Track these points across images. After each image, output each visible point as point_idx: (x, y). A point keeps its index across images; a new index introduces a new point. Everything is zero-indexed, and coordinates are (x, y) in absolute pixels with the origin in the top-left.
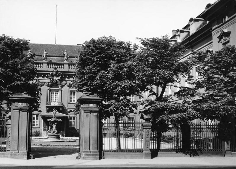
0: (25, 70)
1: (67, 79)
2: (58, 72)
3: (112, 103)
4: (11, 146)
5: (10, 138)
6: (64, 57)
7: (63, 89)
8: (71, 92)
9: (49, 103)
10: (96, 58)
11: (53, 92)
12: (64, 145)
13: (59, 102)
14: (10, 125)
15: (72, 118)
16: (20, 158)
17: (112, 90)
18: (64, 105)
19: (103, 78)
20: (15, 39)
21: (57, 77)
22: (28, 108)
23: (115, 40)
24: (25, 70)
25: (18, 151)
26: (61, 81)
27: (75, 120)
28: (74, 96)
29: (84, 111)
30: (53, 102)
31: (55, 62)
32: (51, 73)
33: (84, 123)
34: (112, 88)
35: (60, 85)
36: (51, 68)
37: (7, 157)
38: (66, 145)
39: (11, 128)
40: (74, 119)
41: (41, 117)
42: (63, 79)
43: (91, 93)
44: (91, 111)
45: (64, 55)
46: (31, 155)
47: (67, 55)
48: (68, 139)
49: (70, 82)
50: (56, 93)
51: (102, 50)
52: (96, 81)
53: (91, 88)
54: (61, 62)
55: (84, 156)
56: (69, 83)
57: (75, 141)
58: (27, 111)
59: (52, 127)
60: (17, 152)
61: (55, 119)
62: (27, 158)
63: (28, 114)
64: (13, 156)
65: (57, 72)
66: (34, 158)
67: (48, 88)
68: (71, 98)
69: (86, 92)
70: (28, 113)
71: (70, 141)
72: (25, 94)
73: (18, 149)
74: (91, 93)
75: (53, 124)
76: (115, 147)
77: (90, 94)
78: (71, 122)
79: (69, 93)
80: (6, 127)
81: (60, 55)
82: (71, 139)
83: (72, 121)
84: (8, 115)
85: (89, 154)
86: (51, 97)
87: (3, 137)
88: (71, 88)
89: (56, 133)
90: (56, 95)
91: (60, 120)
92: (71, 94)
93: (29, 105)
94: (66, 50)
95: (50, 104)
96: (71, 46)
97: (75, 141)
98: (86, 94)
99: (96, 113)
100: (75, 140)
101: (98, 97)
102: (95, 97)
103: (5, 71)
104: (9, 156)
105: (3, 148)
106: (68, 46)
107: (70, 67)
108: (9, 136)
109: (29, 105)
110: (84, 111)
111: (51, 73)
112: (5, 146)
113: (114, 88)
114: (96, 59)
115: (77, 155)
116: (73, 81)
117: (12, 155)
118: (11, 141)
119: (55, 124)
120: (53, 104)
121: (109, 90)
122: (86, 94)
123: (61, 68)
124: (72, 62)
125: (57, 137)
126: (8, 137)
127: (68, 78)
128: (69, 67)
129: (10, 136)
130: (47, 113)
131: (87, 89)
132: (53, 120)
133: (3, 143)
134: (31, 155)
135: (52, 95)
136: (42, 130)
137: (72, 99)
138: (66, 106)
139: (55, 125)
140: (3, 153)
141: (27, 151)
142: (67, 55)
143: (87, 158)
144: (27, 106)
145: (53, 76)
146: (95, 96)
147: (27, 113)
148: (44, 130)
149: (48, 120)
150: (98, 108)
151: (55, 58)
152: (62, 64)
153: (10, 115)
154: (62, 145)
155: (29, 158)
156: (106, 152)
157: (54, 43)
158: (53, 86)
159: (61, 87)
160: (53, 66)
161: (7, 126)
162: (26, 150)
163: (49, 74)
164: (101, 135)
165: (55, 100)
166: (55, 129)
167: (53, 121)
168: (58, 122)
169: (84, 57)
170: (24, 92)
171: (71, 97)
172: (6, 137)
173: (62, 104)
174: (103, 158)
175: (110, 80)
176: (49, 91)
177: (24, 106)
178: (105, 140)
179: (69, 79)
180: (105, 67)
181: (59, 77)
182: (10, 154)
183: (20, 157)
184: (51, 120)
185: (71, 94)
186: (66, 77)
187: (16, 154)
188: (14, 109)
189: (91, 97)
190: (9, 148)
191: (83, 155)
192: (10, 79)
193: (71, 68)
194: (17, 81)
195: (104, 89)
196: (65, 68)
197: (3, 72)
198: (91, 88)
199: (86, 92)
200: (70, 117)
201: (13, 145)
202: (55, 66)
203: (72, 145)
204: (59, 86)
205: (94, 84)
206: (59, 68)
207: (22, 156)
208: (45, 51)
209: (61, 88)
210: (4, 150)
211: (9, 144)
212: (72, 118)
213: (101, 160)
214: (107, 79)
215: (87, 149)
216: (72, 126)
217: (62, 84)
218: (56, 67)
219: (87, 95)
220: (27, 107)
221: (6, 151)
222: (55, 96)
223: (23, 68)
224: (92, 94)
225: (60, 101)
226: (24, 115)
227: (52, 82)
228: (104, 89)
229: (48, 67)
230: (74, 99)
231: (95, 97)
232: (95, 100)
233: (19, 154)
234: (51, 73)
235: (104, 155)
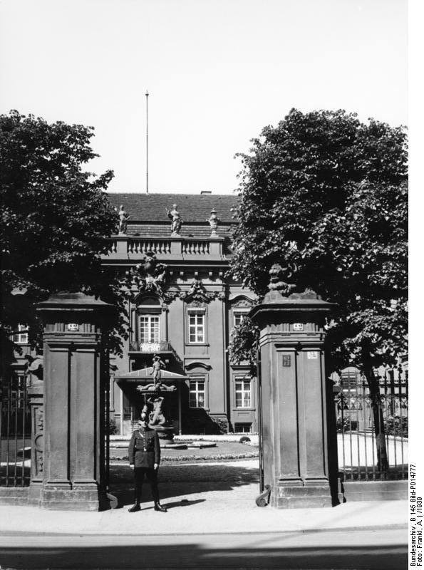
0: (82, 215)
1: (179, 281)
2: (156, 264)
3: (363, 317)
4: (46, 468)
5: (41, 441)
6: (170, 223)
7: (170, 307)
8: (192, 314)
9: (135, 346)
10: (308, 172)
11: (144, 316)
12: (192, 459)
13: (162, 343)
14: (41, 396)
15: (197, 384)
16: (76, 506)
17: (364, 273)
18: (175, 352)
19: (336, 234)
20: (49, 124)
21: (154, 278)
22: (96, 340)
23: (356, 123)
24: (82, 215)
25: (70, 483)
26: (164, 286)
27: (203, 389)
28: (200, 326)
29: (277, 346)
30: (147, 342)
31: (149, 236)
32: (138, 266)
33: (277, 386)
34: (363, 266)
35: (163, 296)
36: (139, 252)
37: (35, 503)
38: (197, 457)
39: (44, 406)
40: (201, 387)
41: (115, 383)
42: (170, 281)
43: (294, 285)
44: (299, 347)
45: (171, 217)
46: (110, 495)
47: (177, 217)
48: (196, 440)
49: (187, 289)
50: (152, 319)
51: (328, 148)
52: (311, 247)
53: (296, 270)
54: (163, 237)
55: (281, 495)
56: (187, 292)
57: (214, 446)
58: (93, 350)
59: (151, 408)
60: (66, 488)
61: (157, 385)
62: (98, 507)
63: (98, 359)
64: (53, 500)
65: (154, 262)
66: (122, 507)
67: (131, 307)
68: (192, 330)
69: (280, 284)
70: (96, 356)
71: (202, 447)
72: (86, 293)
73: (69, 478)
74: (294, 285)
75: (153, 400)
76: (371, 460)
77: (293, 290)
78: (195, 394)
79: (187, 318)
80: (30, 405)
81: (161, 220)
82: (201, 440)
83: (197, 391)
84: (33, 364)
85: (301, 489)
86: (140, 330)
87: (20, 437)
88: (191, 304)
89: (162, 425)
90: (152, 325)
91: (171, 388)
92: (192, 321)
93: (99, 330)
94: (175, 205)
95: (139, 349)
96: (187, 197)
97: (214, 446)
98: (281, 291)
99: (316, 353)
100: (214, 443)
101: (317, 298)
102: (308, 298)
103: (20, 219)
104: (41, 499)
105: (19, 468)
106: (177, 196)
107: (188, 249)
108: (38, 433)
109: (99, 330)
110: (277, 346)
111: (140, 264)
112: (28, 463)
113: (373, 267)
114: (307, 176)
115: (253, 490)
116: (197, 285)
117: (49, 496)
118: (46, 450)
119: (160, 400)
120: (146, 348)
121: (354, 273)
122: (279, 288)
123: (165, 251)
124: (192, 236)
125: (166, 435)
126: (37, 438)
127: (184, 278)
128: (184, 249)
129: (42, 432)
130: (132, 372)
131: (281, 272)
132: (153, 388)
133: (20, 454)
134: (110, 495)
135: (142, 325)
136: (121, 417)
137: (194, 332)
138: (180, 353)
139: (160, 403)
140: (21, 489)
141: (96, 483)
142: (177, 217)
143: (293, 500)
144: (93, 332)
145: (143, 272)
146: (309, 297)
147: (93, 355)
148: (126, 417)
149: (141, 388)
150: (321, 334)
151: (149, 226)
152: (167, 242)
153: (40, 366)
154: (186, 459)
155: (104, 506)
156: (348, 477)
157: (143, 191)
158: (145, 299)
159: (165, 302)
160: (144, 248)
161: (33, 401)
162: (95, 479)
163: (134, 268)
164: (334, 428)
165: (150, 339)
166: (160, 414)
167: (154, 392)
168: (166, 394)
169: (268, 170)
170: (83, 289)
171: (191, 328)
172: (28, 435)
173: (170, 348)
174: (341, 501)
175: (358, 240)
176: (134, 313)
177: (83, 335)
178: (343, 441)
179: (186, 280)
180: (338, 200)
181: (160, 277)
182: (44, 495)
183: (76, 503)
184: (147, 389)
185: (192, 321)
186: (177, 275)
187: (62, 494)
188: (52, 346)
189: (297, 299)
190: (40, 473)
191: (279, 492)
192: (35, 246)
193: (190, 251)
194: (61, 252)
195: (340, 269)
196: (176, 253)
197: (14, 221)
198: (296, 270)
199: (280, 284)
200: (190, 382)
201: (54, 463)
202: (148, 248)
203: (214, 459)
204: (161, 301)
205: (303, 257)
206: (158, 252)
207: (83, 500)
208: (123, 209)
209: (165, 304)
210: (20, 478)
211: (40, 462)
212: (197, 384)
213: (338, 507)
214: (348, 237)
215: (290, 472)
216: (197, 406)
217: (167, 294)
218: (150, 250)
219: (285, 291)
220: (94, 337)
221: (31, 483)
222: (149, 327)
223: (77, 209)
224: (299, 290)
225: (165, 340)
226: (85, 362)
227: (143, 290)
228: (340, 269)
229: (132, 251)
230: (200, 335)
231: (308, 298)
232: (310, 309)
233: (72, 495)
234: (138, 266)
235: (343, 491)
